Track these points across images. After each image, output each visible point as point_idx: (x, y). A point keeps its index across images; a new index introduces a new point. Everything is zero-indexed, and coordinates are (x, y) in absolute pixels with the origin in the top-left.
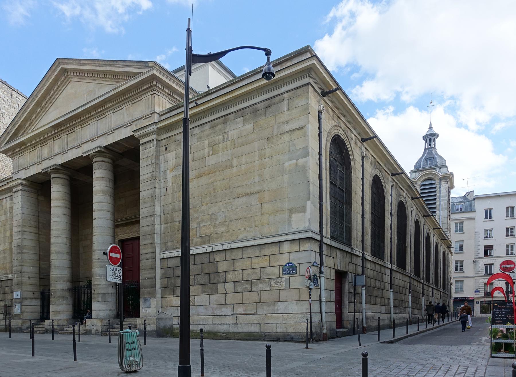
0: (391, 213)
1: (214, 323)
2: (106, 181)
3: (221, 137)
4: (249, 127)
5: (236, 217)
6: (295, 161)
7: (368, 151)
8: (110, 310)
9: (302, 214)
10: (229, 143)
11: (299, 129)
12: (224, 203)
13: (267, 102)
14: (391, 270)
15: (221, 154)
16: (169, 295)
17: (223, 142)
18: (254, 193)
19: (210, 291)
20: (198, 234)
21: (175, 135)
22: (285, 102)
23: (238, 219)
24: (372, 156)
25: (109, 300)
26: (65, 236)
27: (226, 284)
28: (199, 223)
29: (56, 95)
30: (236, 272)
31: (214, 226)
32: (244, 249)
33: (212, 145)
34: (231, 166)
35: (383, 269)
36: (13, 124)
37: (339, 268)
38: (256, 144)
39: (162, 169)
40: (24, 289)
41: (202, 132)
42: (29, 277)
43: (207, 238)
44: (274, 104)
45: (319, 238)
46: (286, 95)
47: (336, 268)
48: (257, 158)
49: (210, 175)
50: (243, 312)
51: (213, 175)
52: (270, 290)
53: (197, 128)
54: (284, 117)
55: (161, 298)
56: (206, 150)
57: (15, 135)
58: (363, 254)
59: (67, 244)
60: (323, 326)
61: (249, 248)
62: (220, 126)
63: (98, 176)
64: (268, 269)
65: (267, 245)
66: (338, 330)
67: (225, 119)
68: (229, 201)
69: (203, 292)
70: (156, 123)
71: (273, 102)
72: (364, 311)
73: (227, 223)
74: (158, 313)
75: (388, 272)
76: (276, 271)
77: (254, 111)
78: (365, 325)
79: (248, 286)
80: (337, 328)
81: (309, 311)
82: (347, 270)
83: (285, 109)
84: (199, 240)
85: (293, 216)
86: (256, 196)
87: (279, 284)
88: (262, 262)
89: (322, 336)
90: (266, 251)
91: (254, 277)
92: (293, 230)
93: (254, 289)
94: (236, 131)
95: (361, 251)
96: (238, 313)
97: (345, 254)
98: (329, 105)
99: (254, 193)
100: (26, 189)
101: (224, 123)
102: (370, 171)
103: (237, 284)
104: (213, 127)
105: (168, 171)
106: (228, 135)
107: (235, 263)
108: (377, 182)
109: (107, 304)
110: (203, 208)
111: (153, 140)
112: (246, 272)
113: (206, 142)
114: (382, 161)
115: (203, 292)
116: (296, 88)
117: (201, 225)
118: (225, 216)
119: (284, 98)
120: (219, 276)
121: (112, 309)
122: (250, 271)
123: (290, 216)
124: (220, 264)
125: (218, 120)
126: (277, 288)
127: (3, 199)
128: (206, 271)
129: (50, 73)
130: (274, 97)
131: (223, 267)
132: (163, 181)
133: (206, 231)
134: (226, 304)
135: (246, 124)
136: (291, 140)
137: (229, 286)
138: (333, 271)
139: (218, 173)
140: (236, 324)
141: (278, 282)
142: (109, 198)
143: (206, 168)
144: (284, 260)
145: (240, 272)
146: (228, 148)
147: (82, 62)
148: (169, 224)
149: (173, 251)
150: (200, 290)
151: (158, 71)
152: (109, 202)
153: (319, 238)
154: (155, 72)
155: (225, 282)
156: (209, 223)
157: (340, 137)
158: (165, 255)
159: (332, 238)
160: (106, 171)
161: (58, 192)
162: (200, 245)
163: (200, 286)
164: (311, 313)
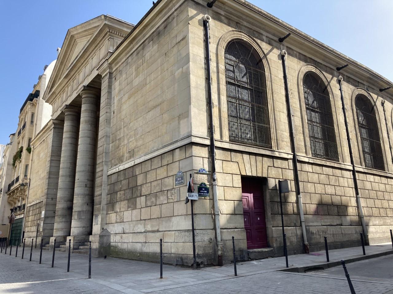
0: (343, 108)
1: (134, 241)
2: (89, 113)
3: (141, 60)
4: (156, 47)
5: (148, 130)
6: (181, 69)
7: (292, 50)
8: (84, 227)
9: (187, 119)
10: (145, 64)
11: (183, 39)
12: (142, 118)
13: (165, 23)
14: (354, 172)
15: (141, 75)
16: (110, 211)
17: (142, 65)
18: (158, 105)
19: (132, 206)
20: (128, 149)
21: (120, 66)
22: (175, 19)
23: (149, 132)
24: (300, 53)
25: (83, 217)
26: (69, 161)
27: (142, 197)
28: (128, 140)
29: (71, 55)
30: (147, 185)
31: (136, 140)
32: (152, 160)
33: (137, 69)
34: (146, 84)
35: (338, 172)
36: (51, 81)
37: (249, 174)
38: (159, 61)
39: (113, 96)
40: (284, 201)
41: (132, 59)
42: (52, 198)
43: (132, 152)
44: (169, 23)
45: (208, 142)
46: (175, 14)
47: (244, 173)
48: (159, 73)
49: (135, 95)
50: (150, 229)
51: (137, 94)
52: (168, 203)
53: (130, 57)
54: (174, 32)
55: (107, 214)
56: (134, 74)
57: (52, 87)
58: (294, 156)
59: (71, 168)
60: (217, 246)
61: (155, 159)
62: (141, 52)
63: (83, 109)
64: (166, 180)
65: (165, 154)
66: (249, 250)
67: (143, 45)
68: (144, 116)
69: (128, 207)
70: (107, 60)
71: (168, 22)
72: (303, 224)
73: (143, 136)
74: (102, 230)
75: (349, 174)
76: (170, 182)
77: (158, 34)
78: (306, 243)
79: (153, 199)
80: (248, 248)
81: (191, 228)
82: (265, 175)
83: (175, 25)
84: (128, 155)
85: (181, 122)
86: (159, 108)
87: (173, 196)
88: (162, 173)
89: (217, 259)
90: (165, 162)
91: (158, 189)
92: (181, 137)
93: (158, 203)
94: (149, 53)
95: (290, 152)
96: (148, 230)
97: (260, 158)
98: (220, 14)
99: (158, 105)
100: (57, 126)
101: (143, 49)
102: (297, 68)
103: (148, 198)
104: (138, 54)
105: (115, 97)
106: (145, 58)
107: (147, 176)
108: (310, 80)
109: (81, 221)
110: (131, 124)
111: (107, 74)
112: (153, 184)
113: (134, 67)
114: (317, 57)
115: (128, 207)
116: (180, 6)
117: (130, 141)
118: (142, 130)
119: (174, 16)
120: (137, 190)
121: (85, 226)
122: (156, 182)
123: (179, 123)
124: (138, 178)
125: (139, 48)
126: (172, 201)
127: (47, 136)
128: (131, 186)
129: (66, 40)
130: (169, 17)
131: (140, 180)
132: (112, 106)
133: (132, 146)
134: (141, 220)
135: (154, 45)
136: (179, 51)
137: (143, 198)
138: (240, 177)
139: (139, 92)
140: (146, 243)
141: (172, 194)
142: (89, 126)
143: (133, 89)
144: (175, 169)
145: (150, 184)
146: (145, 69)
147: (78, 27)
148: (114, 143)
149: (115, 167)
150: (127, 205)
151: (109, 21)
152: (89, 129)
153: (208, 142)
154: (107, 22)
155: (141, 196)
156: (133, 139)
157: (243, 40)
158: (110, 172)
159: (233, 140)
160: (89, 105)
161: (67, 126)
162: (129, 159)
163: (127, 201)
164: (193, 230)
